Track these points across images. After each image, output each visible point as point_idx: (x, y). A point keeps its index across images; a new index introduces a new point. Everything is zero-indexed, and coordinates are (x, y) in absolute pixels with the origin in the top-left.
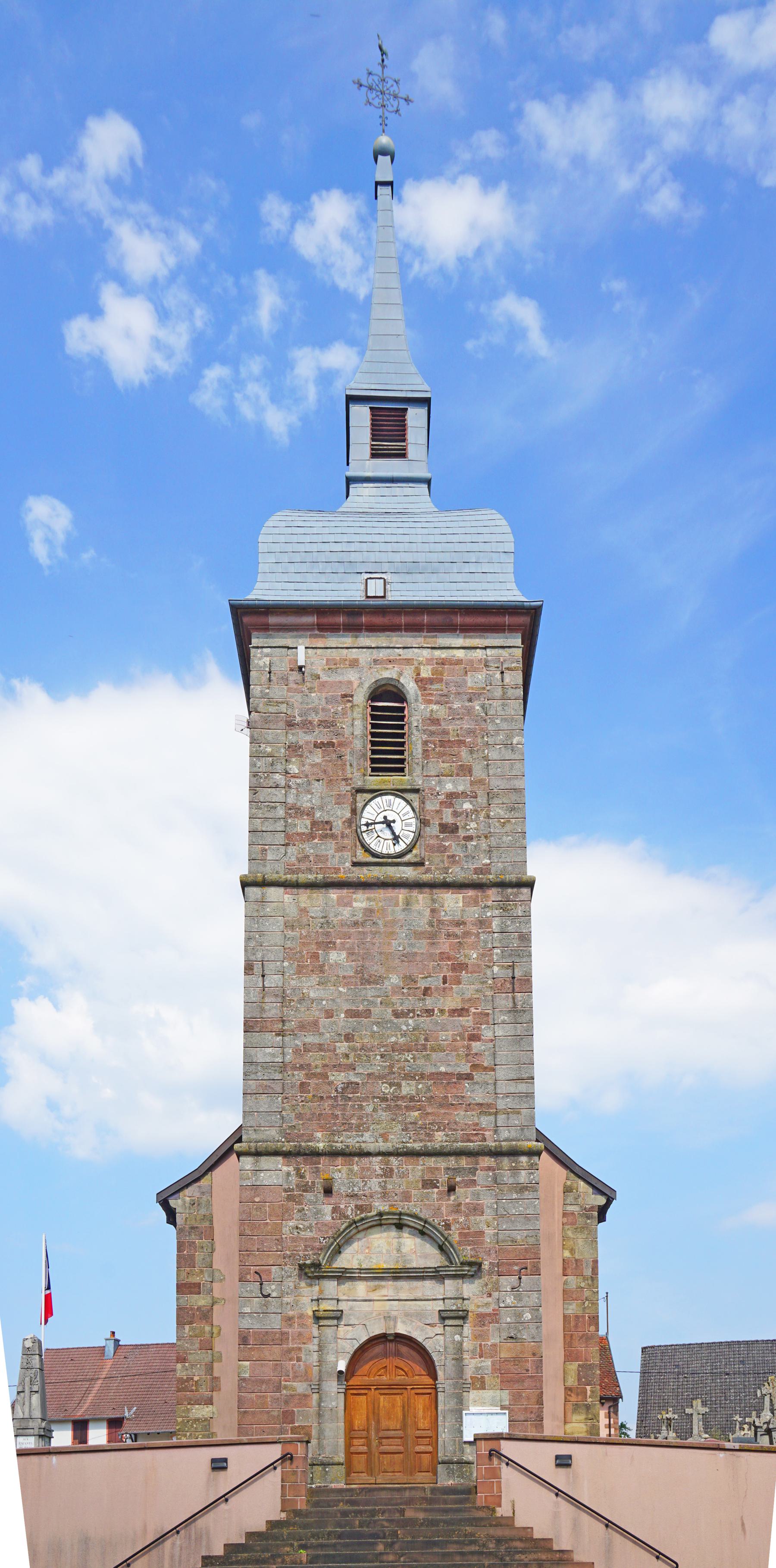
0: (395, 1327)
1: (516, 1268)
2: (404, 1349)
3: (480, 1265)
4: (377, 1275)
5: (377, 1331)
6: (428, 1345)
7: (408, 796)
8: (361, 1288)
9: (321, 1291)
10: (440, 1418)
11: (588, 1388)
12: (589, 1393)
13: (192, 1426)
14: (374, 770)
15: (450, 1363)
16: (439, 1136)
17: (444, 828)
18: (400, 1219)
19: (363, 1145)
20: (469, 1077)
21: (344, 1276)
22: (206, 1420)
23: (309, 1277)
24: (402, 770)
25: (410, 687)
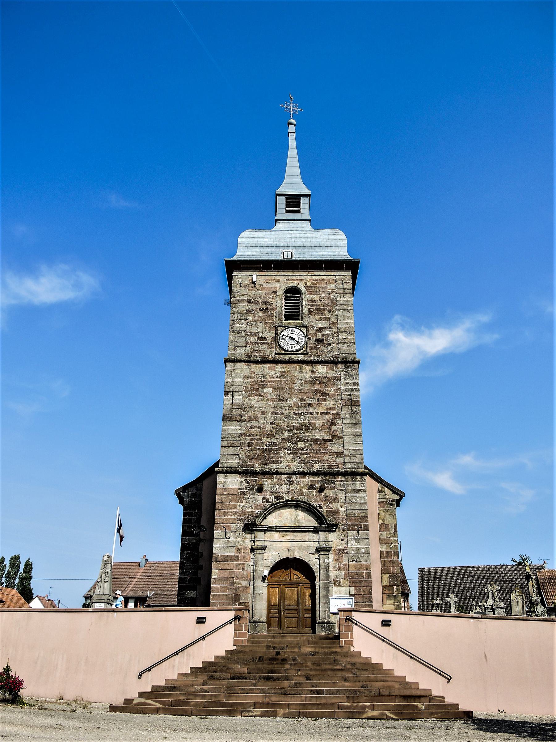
1: (356, 527)
7: (301, 328)
11: (395, 587)
12: (395, 589)
21: (267, 530)
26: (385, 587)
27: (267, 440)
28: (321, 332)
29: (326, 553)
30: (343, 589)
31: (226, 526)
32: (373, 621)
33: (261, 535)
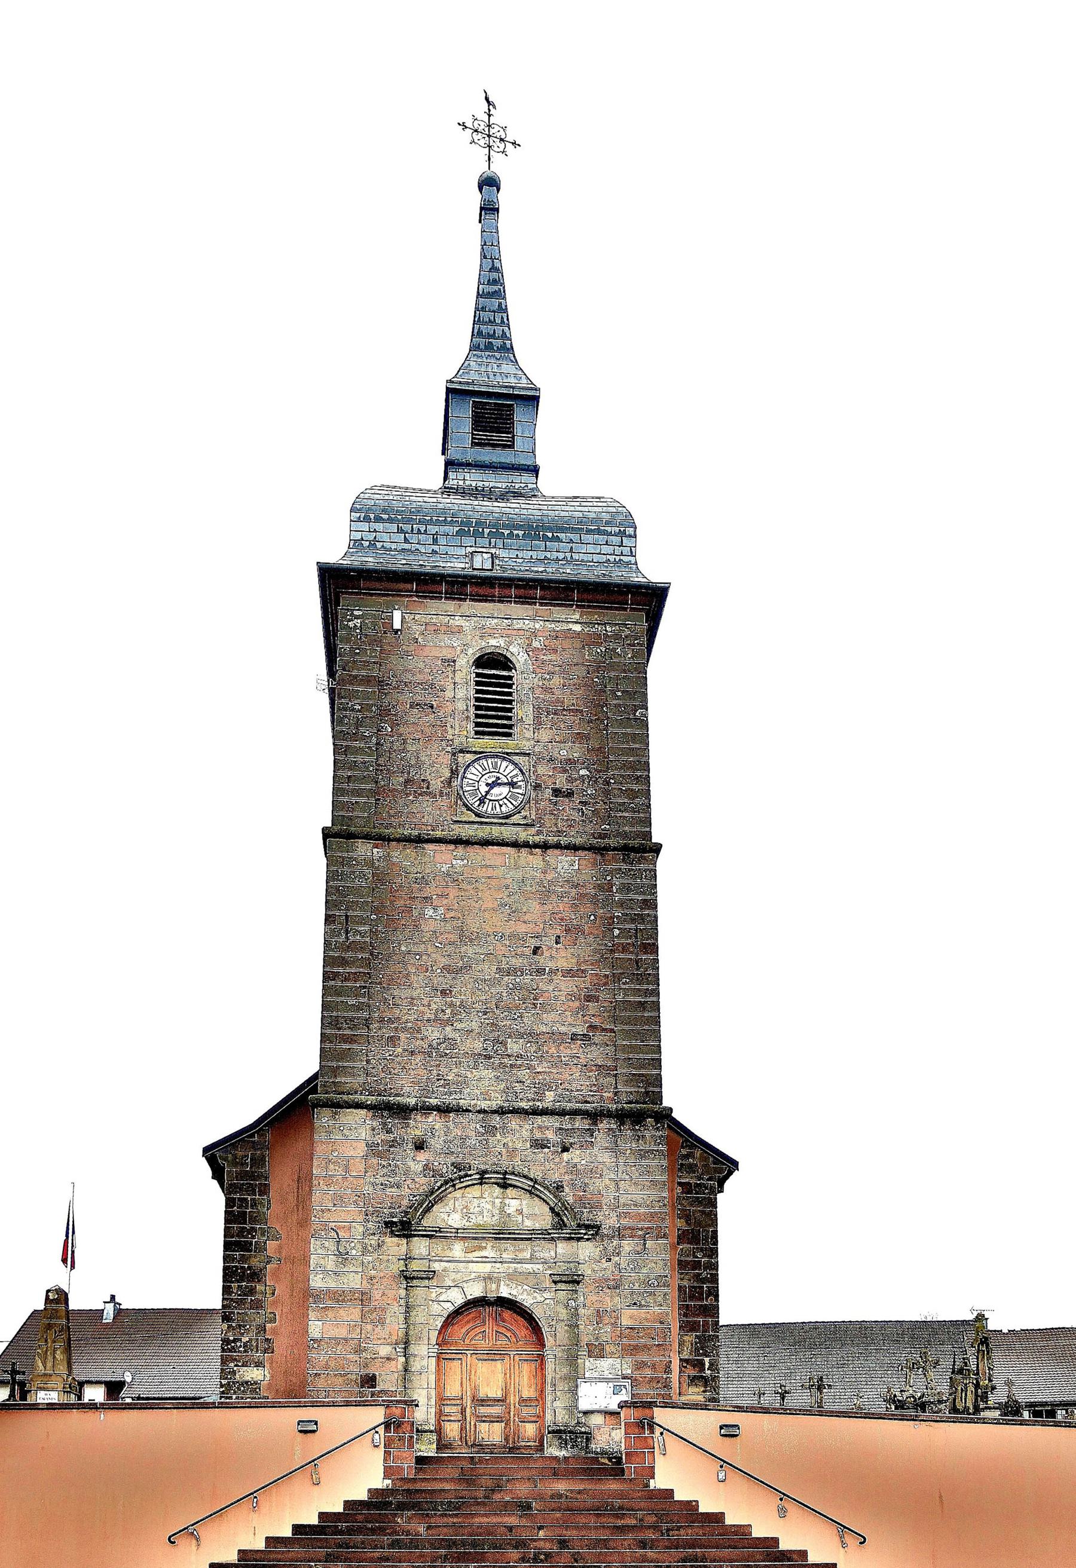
0: (498, 1289)
1: (640, 1233)
2: (507, 1314)
3: (598, 1227)
4: (474, 1237)
5: (475, 1291)
6: (538, 1313)
7: (516, 758)
8: (458, 1250)
9: (409, 1250)
10: (549, 1388)
11: (707, 1360)
12: (707, 1365)
13: (239, 1389)
14: (477, 733)
15: (562, 1330)
16: (550, 1096)
17: (557, 792)
18: (505, 1178)
19: (462, 1102)
20: (390, 1147)
21: (434, 1234)
22: (256, 1383)
23: (397, 1236)
24: (509, 735)
25: (519, 656)
26: (687, 1361)
27: (433, 1034)
28: (565, 771)
29: (570, 1287)
30: (606, 1365)
31: (339, 1228)
32: (701, 1425)
33: (420, 1246)
